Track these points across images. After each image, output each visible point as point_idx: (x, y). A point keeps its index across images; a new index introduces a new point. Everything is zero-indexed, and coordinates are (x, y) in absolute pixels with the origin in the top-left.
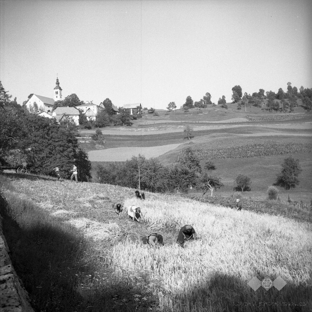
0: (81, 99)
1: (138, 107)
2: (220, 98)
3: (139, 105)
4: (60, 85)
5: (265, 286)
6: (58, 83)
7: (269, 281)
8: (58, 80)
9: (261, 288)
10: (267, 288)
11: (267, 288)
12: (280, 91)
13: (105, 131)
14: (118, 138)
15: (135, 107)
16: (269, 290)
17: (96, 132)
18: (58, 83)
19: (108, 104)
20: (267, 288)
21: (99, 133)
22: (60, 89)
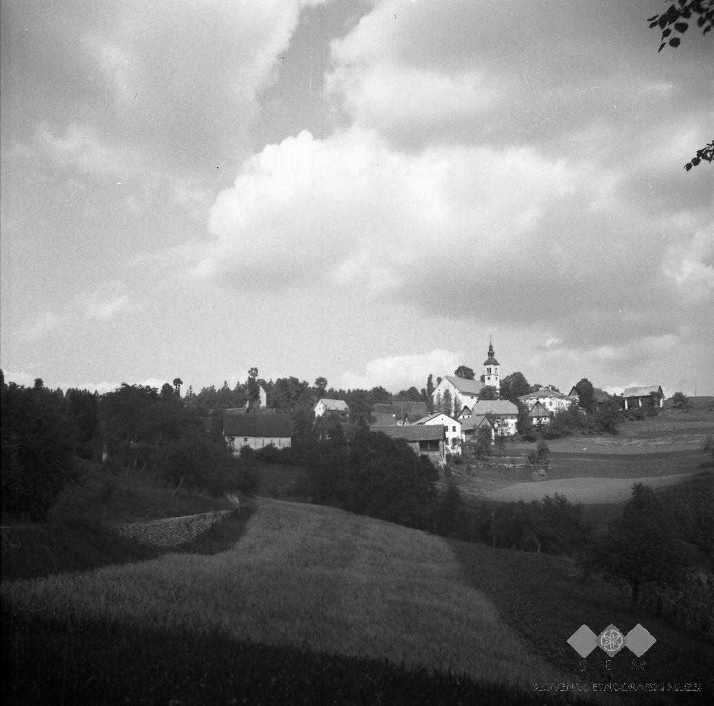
0: (531, 382)
1: (653, 394)
2: (178, 382)
3: (656, 390)
4: (496, 357)
5: (606, 647)
6: (491, 354)
7: (616, 634)
8: (491, 348)
9: (598, 652)
10: (612, 651)
11: (612, 651)
12: (271, 382)
13: (554, 446)
14: (580, 460)
15: (646, 393)
16: (616, 655)
17: (538, 447)
18: (491, 354)
19: (584, 390)
20: (611, 650)
21: (543, 451)
22: (496, 363)
